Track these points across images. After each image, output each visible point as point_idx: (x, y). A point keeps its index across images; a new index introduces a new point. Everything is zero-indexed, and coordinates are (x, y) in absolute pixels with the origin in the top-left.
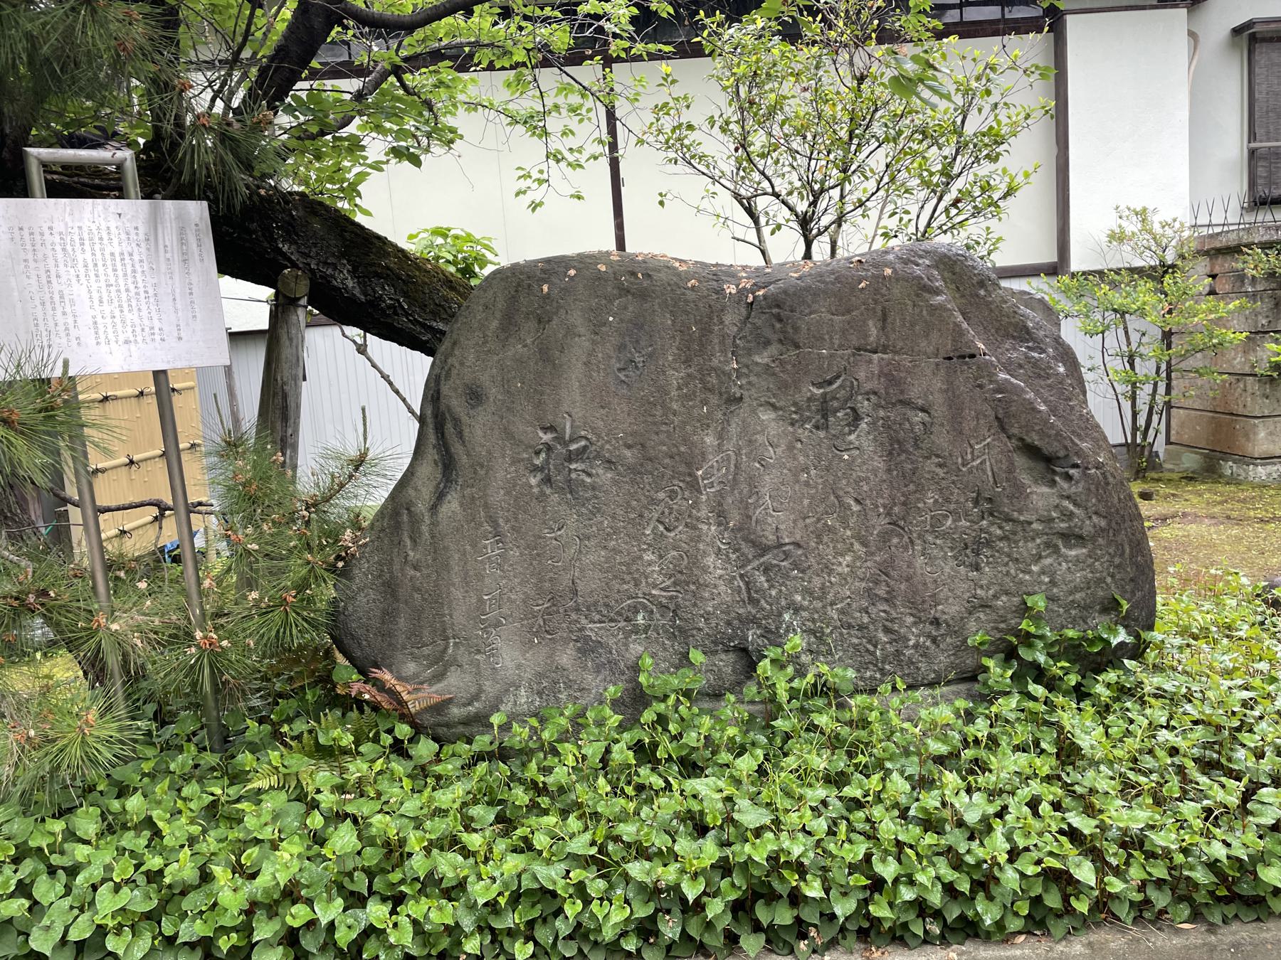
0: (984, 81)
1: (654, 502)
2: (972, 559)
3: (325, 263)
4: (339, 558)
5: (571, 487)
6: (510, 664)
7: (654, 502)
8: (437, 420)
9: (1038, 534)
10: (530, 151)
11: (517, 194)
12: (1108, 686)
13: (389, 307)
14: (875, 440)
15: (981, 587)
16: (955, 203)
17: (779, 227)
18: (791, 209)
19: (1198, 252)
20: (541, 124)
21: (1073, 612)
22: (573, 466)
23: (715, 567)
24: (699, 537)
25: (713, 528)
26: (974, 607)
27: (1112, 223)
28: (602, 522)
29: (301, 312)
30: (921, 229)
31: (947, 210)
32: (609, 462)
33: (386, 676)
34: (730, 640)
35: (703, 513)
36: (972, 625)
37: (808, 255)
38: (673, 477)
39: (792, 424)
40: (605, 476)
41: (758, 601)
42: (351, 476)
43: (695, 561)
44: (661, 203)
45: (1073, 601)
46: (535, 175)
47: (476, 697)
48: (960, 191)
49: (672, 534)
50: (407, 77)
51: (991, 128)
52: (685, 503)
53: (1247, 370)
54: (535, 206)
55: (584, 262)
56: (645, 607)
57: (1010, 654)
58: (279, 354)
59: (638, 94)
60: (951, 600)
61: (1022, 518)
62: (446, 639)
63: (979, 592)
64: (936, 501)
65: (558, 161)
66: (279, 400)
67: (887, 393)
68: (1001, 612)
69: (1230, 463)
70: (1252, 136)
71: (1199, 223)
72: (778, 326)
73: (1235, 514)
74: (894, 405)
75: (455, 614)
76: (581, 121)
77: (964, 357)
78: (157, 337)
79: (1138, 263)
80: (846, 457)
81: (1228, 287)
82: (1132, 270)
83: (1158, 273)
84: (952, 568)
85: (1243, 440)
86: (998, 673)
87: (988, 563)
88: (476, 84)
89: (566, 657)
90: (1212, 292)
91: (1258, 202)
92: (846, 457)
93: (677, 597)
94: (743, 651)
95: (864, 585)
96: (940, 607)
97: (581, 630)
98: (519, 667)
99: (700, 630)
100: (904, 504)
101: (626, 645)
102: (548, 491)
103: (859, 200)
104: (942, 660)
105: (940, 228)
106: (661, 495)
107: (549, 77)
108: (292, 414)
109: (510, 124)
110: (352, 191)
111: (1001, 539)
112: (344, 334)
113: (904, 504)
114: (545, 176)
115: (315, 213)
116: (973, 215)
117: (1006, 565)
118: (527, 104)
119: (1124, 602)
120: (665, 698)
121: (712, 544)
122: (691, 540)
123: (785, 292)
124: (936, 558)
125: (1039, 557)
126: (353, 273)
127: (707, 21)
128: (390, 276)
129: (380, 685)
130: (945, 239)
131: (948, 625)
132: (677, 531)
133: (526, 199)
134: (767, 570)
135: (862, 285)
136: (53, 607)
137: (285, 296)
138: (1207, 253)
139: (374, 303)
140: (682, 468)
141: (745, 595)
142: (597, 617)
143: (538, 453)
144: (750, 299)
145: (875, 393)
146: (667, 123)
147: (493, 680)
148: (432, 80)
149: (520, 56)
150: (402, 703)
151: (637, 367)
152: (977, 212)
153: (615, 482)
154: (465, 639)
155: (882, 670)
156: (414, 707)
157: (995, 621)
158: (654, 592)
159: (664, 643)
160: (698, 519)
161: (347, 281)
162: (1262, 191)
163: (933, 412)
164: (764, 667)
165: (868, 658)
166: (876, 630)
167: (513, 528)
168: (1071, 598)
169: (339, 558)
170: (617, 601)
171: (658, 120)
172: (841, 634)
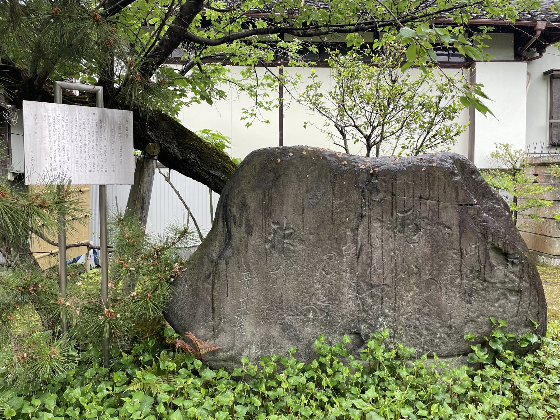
0: (449, 86)
1: (322, 260)
2: (468, 298)
3: (166, 141)
4: (172, 276)
5: (283, 251)
6: (249, 333)
7: (322, 260)
8: (223, 215)
9: (499, 289)
10: (249, 102)
11: (241, 119)
12: (529, 362)
13: (192, 162)
14: (425, 239)
15: (472, 312)
16: (434, 136)
17: (358, 140)
18: (362, 133)
19: (530, 164)
20: (255, 90)
21: (512, 326)
22: (285, 241)
23: (348, 294)
24: (341, 278)
25: (348, 275)
26: (468, 321)
27: (493, 149)
28: (296, 268)
29: (154, 161)
30: (419, 146)
31: (430, 139)
32: (302, 240)
33: (191, 335)
34: (352, 329)
35: (344, 267)
36: (466, 329)
37: (368, 155)
38: (331, 250)
39: (388, 229)
40: (300, 247)
41: (368, 311)
42: (179, 239)
43: (339, 289)
44: (305, 127)
45: (512, 321)
46: (250, 112)
47: (231, 348)
48: (437, 131)
49: (329, 276)
50: (203, 66)
51: (450, 106)
52: (336, 262)
53: (551, 217)
54: (248, 125)
55: (274, 150)
56: (313, 310)
57: (484, 344)
58: (143, 180)
59: (297, 82)
60: (457, 317)
61: (492, 281)
62: (220, 319)
63: (470, 314)
64: (452, 270)
65: (260, 106)
66: (140, 200)
67: (432, 219)
68: (480, 324)
69: (543, 257)
70: (551, 117)
71: (530, 152)
72: (384, 184)
73: (548, 280)
74: (435, 224)
75: (226, 307)
76: (272, 90)
77: (467, 205)
78: (103, 170)
79: (504, 167)
80: (412, 246)
81: (542, 180)
82: (502, 170)
83: (513, 172)
84: (459, 302)
85: (549, 247)
86: (481, 355)
87: (475, 301)
88: (233, 72)
89: (275, 332)
90: (535, 182)
91: (553, 145)
92: (412, 246)
93: (329, 306)
94: (357, 334)
95: (418, 307)
96: (452, 320)
97: (283, 319)
98: (253, 335)
99: (339, 323)
100: (438, 270)
101: (303, 327)
102: (273, 252)
103: (393, 132)
104: (451, 345)
105: (427, 146)
106: (325, 257)
107: (261, 70)
108: (146, 207)
109: (240, 90)
110: (176, 111)
111: (482, 290)
112: (160, 172)
113: (438, 270)
114: (254, 112)
115: (164, 120)
116: (442, 142)
117: (484, 302)
118: (250, 82)
119: (536, 323)
120: (325, 356)
121: (348, 282)
122: (338, 280)
123: (388, 169)
124: (451, 297)
125: (498, 299)
126: (178, 146)
127: (331, 53)
128: (193, 149)
129: (189, 341)
130: (429, 151)
131: (456, 329)
132: (331, 275)
133: (245, 122)
134: (372, 296)
135: (423, 169)
136: (40, 292)
137: (148, 155)
138: (534, 165)
139: (186, 160)
140: (335, 245)
141: (361, 308)
142: (291, 313)
143: (270, 234)
144: (371, 171)
145: (427, 218)
146: (312, 93)
147: (241, 340)
148: (213, 68)
149: (250, 61)
150: (195, 347)
151: (317, 198)
152: (444, 140)
153: (304, 250)
154: (229, 320)
155: (423, 348)
156: (203, 352)
157: (477, 328)
158: (318, 303)
159: (321, 328)
160: (341, 270)
161: (175, 150)
162: (556, 141)
163: (453, 229)
164: (371, 344)
165: (417, 342)
166: (422, 329)
167: (256, 268)
168: (512, 320)
169: (172, 276)
170: (301, 306)
171: (308, 92)
172: (406, 329)
